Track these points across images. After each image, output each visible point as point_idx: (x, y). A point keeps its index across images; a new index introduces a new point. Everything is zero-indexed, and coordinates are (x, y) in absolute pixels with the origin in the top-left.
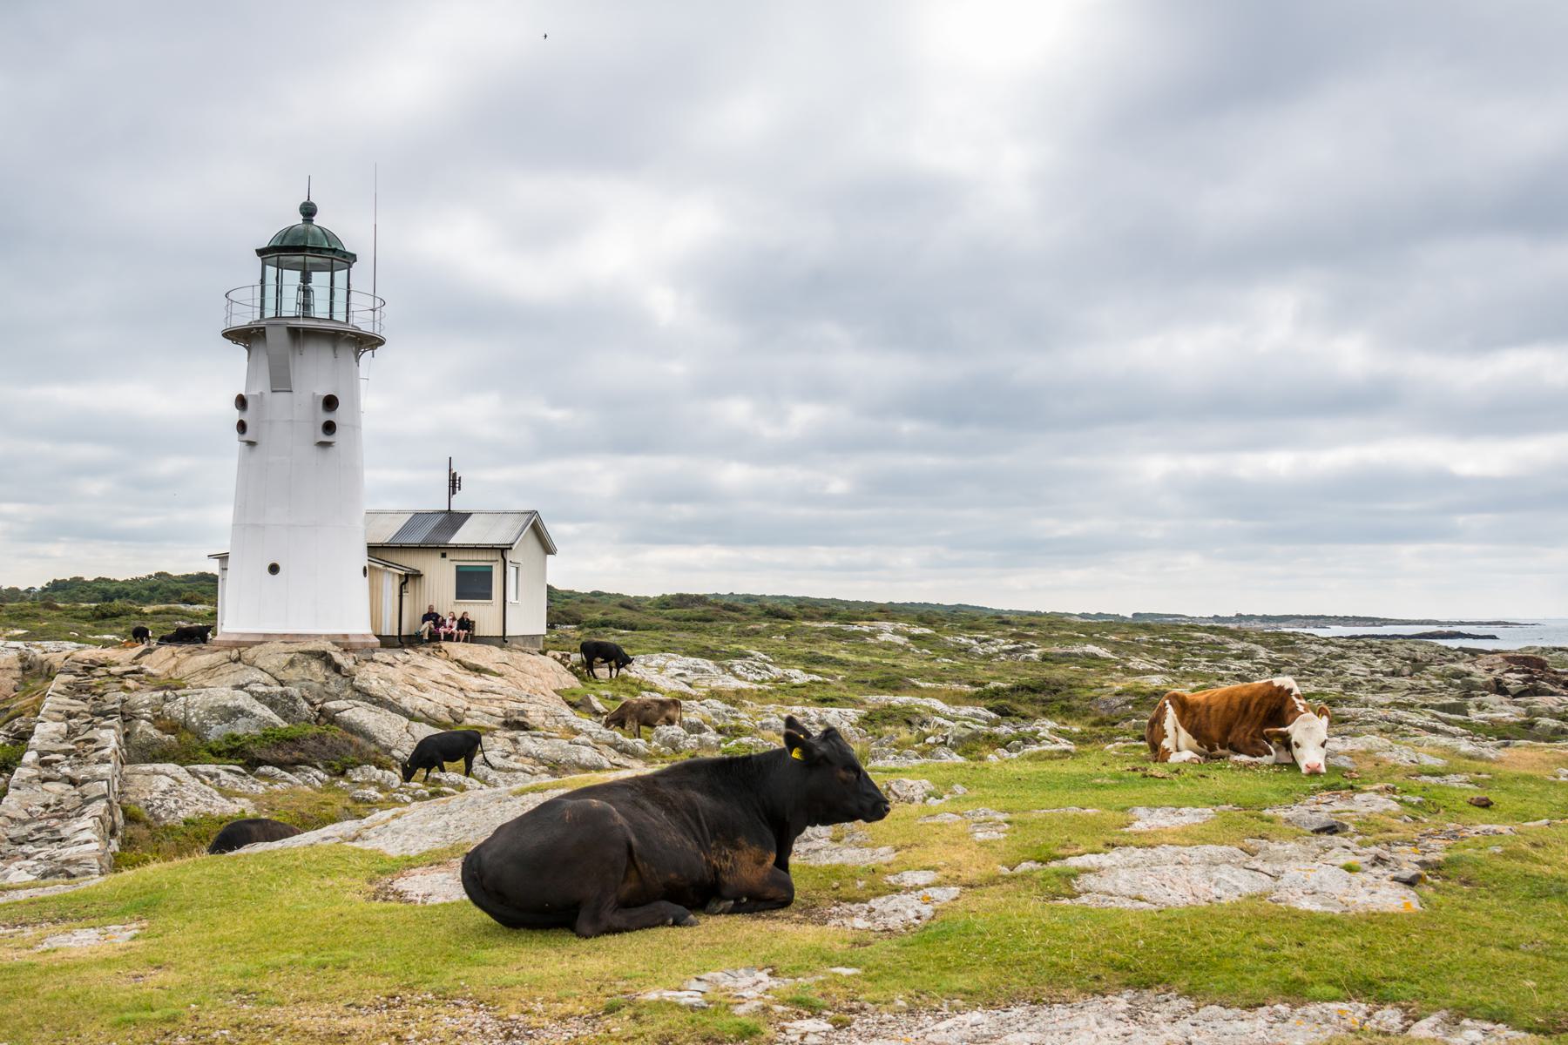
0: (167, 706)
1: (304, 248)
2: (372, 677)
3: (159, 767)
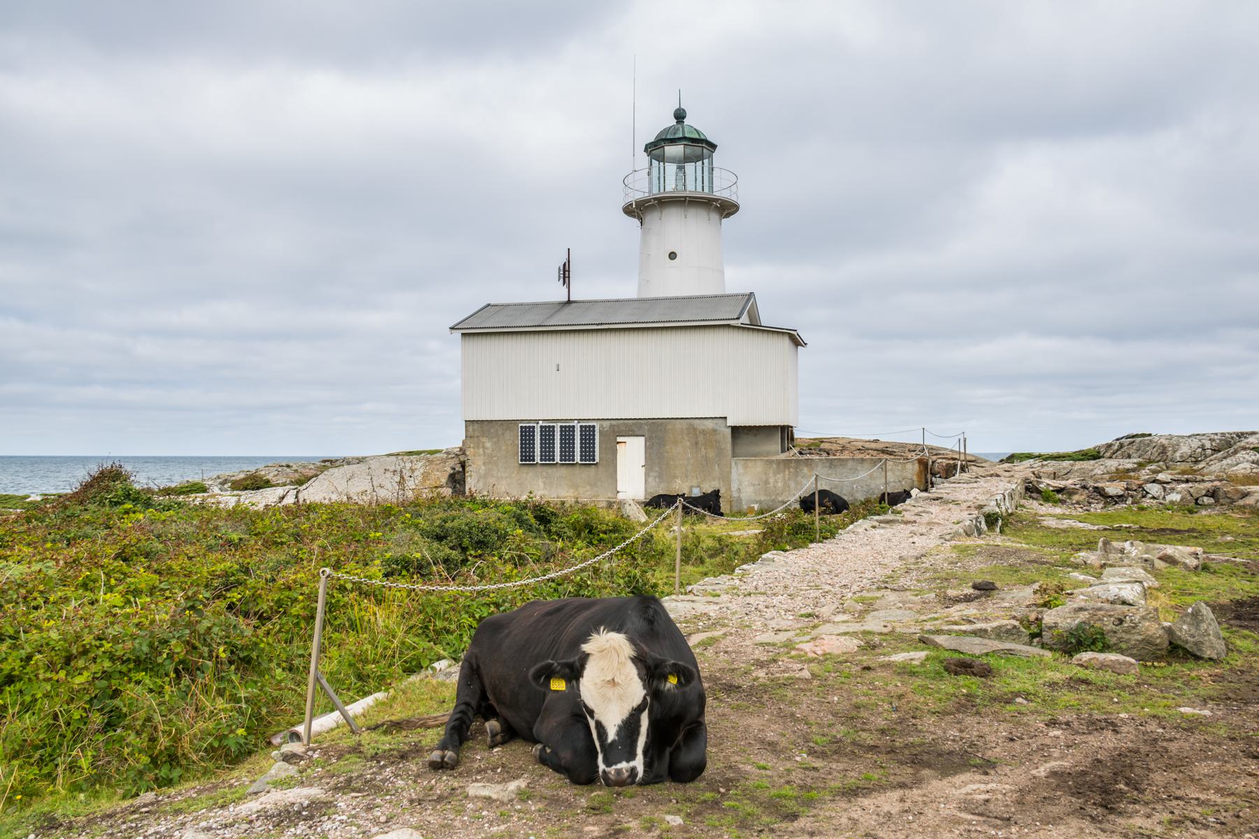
1: (682, 142)
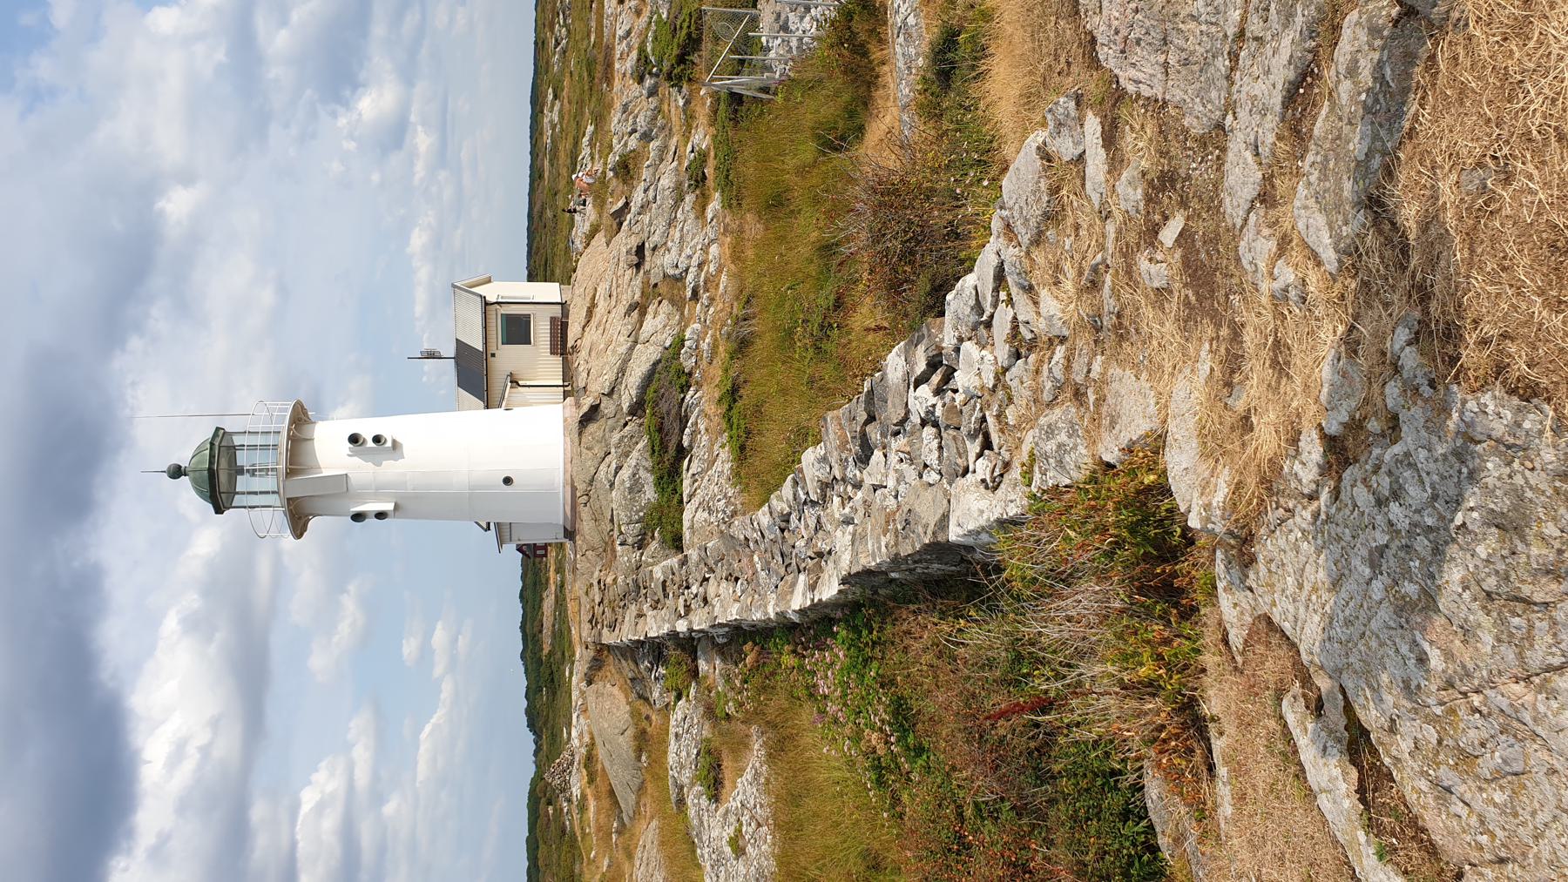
0: (630, 540)
2: (598, 385)
3: (686, 524)
